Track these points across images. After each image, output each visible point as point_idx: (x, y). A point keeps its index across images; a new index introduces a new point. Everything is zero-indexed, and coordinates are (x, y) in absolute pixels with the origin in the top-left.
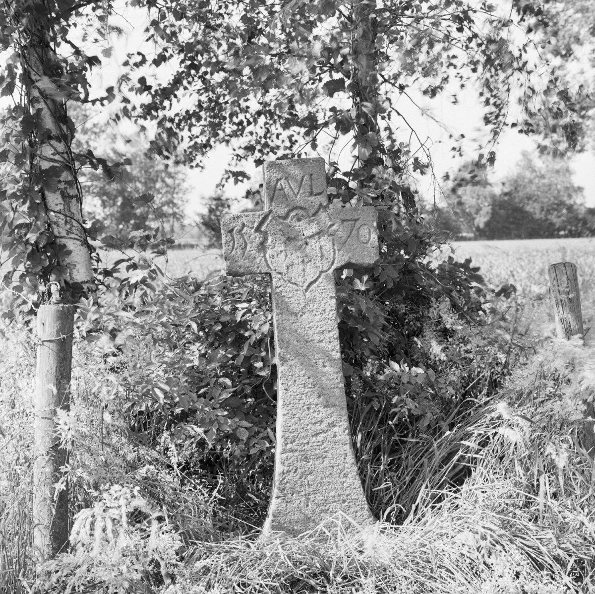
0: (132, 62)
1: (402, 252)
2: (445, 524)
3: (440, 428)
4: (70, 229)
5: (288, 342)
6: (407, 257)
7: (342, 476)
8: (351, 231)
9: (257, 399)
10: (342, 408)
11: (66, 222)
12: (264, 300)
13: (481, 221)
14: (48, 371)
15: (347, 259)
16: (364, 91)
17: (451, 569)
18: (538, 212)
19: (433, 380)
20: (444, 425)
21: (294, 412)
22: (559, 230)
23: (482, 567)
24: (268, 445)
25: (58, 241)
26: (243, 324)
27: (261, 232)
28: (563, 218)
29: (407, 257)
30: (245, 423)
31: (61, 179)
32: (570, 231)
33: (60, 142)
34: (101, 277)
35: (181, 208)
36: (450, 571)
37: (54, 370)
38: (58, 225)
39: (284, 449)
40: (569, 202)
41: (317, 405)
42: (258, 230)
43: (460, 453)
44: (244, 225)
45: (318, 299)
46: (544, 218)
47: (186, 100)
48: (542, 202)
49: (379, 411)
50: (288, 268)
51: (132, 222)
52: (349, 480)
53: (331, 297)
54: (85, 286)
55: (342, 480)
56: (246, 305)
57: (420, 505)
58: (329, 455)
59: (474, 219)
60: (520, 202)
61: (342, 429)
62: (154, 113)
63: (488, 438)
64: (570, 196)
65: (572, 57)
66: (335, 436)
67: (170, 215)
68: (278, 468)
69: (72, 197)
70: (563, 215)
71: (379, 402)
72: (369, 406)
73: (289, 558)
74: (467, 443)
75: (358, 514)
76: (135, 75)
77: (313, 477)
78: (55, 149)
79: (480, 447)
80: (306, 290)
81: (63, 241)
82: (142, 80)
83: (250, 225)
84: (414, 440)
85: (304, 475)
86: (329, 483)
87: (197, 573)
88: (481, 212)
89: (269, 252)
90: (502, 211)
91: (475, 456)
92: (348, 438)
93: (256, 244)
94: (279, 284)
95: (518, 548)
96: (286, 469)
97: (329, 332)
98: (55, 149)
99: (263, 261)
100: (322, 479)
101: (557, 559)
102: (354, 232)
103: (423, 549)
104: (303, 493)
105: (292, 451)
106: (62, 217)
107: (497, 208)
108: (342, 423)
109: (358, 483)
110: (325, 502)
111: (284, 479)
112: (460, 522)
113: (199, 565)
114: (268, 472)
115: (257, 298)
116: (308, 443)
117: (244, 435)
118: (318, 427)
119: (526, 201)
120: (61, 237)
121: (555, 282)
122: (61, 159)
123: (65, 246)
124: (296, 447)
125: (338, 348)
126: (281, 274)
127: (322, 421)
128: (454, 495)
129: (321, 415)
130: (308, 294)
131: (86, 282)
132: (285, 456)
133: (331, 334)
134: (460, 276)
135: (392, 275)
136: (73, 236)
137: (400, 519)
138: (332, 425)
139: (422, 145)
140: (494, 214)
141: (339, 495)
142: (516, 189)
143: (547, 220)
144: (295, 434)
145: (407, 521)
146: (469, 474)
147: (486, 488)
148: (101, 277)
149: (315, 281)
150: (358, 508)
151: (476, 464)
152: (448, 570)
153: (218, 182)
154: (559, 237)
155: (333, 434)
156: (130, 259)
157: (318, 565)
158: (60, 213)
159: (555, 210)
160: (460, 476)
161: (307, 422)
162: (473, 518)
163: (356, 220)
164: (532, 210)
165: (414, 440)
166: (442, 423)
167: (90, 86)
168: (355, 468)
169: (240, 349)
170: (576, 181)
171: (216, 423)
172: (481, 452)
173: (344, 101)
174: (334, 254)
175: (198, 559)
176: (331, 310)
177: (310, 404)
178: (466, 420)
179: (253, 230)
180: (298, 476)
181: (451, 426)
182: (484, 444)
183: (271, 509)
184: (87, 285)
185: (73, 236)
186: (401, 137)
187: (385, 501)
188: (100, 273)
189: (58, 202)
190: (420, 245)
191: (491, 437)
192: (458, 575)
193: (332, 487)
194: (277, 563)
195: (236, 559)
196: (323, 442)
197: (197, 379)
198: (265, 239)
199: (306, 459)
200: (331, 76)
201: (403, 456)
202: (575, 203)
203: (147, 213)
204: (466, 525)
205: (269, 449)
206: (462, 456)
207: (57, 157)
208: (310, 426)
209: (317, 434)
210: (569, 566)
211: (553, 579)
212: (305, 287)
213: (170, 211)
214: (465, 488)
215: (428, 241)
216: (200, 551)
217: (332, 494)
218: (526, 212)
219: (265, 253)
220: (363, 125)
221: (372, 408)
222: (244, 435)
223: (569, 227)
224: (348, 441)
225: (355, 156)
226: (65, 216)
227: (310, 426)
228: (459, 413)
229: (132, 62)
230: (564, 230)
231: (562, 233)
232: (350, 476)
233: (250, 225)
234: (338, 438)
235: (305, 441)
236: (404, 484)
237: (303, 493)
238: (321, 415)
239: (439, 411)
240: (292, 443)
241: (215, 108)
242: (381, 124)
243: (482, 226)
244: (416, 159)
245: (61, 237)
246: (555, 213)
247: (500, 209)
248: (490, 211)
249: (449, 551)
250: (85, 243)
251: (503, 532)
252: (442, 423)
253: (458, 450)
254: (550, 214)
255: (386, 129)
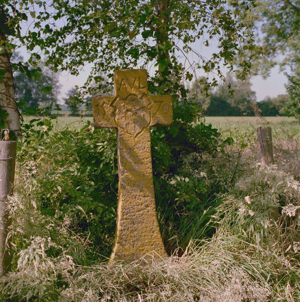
0: (42, 16)
1: (180, 120)
2: (205, 257)
3: (200, 208)
4: (9, 102)
5: (126, 163)
6: (182, 122)
7: (151, 232)
8: (159, 107)
9: (108, 193)
10: (153, 198)
11: (7, 99)
12: (113, 141)
13: (205, 107)
14: (2, 176)
15: (157, 121)
16: (162, 37)
17: (209, 280)
18: (233, 103)
19: (197, 184)
20: (202, 207)
21: (128, 199)
22: (243, 112)
23: (225, 279)
24: (113, 216)
25: (2, 108)
26: (101, 154)
27: (113, 106)
28: (245, 107)
29: (182, 122)
30: (101, 205)
31: (5, 76)
32: (248, 113)
33: (5, 57)
34: (23, 128)
35: (55, 96)
36: (209, 282)
37: (5, 176)
38: (3, 100)
39: (122, 218)
40: (248, 99)
41: (139, 196)
42: (111, 105)
43: (210, 221)
44: (104, 103)
45: (141, 142)
46: (236, 106)
47: (70, 38)
48: (235, 98)
49: (168, 200)
50: (126, 126)
51: (30, 102)
52: (155, 234)
53: (148, 141)
54: (16, 133)
55: (151, 234)
56: (102, 144)
57: (190, 247)
58: (145, 221)
59: (202, 106)
60: (225, 98)
61: (152, 208)
62: (53, 44)
63: (224, 214)
64: (249, 96)
65: (254, 27)
66: (148, 212)
67: (50, 99)
68: (119, 227)
69: (10, 86)
70: (245, 105)
71: (169, 195)
72: (164, 197)
73: (127, 274)
74: (213, 216)
75: (159, 252)
76: (43, 24)
77: (137, 232)
78: (2, 60)
79: (220, 219)
80: (136, 137)
81: (5, 108)
82: (47, 26)
83: (108, 103)
84: (186, 214)
85: (132, 231)
86: (145, 236)
87: (80, 282)
88: (205, 103)
89: (117, 117)
90: (216, 102)
91: (218, 222)
92: (155, 212)
93: (110, 113)
94: (121, 134)
95: (243, 269)
96: (123, 228)
97: (147, 158)
98: (2, 60)
99: (114, 121)
100: (141, 233)
101: (262, 274)
102: (161, 107)
103: (193, 270)
104: (131, 241)
105: (126, 219)
106: (5, 96)
107: (213, 100)
108: (152, 205)
109: (159, 236)
110: (143, 245)
111: (122, 233)
112: (212, 256)
113: (80, 278)
114: (112, 229)
115: (107, 141)
116: (134, 215)
117: (100, 211)
118: (140, 207)
119: (227, 97)
120: (4, 107)
121: (261, 136)
122: (5, 66)
123: (6, 111)
124: (128, 217)
125: (151, 167)
126: (123, 128)
127: (142, 204)
128: (209, 242)
129: (141, 201)
130: (136, 139)
131: (17, 131)
132: (122, 221)
133: (148, 160)
134: (209, 132)
135: (175, 132)
136: (10, 106)
137: (180, 254)
138: (147, 206)
139: (191, 65)
140: (212, 103)
141: (150, 242)
142: (223, 91)
143: (237, 107)
144: (128, 210)
145: (184, 255)
146: (215, 231)
147: (223, 239)
148: (23, 128)
149: (140, 132)
150: (159, 248)
151: (218, 226)
152: (208, 281)
153: (86, 82)
154: (244, 116)
155: (147, 210)
156: (39, 120)
157: (141, 278)
158: (4, 94)
159: (241, 102)
160: (210, 233)
161: (134, 204)
162: (219, 254)
163: (162, 102)
164: (230, 102)
165: (186, 214)
166: (201, 206)
167: (21, 28)
168: (158, 228)
169: (98, 166)
170: (253, 89)
171: (87, 204)
172: (221, 221)
173: (152, 42)
174: (150, 119)
175: (80, 275)
176: (148, 148)
177: (136, 195)
178: (215, 205)
179: (109, 105)
180: (129, 232)
181: (206, 208)
182: (222, 217)
183: (115, 249)
184: (17, 132)
185: (10, 106)
186: (180, 61)
187: (171, 245)
188: (24, 126)
189: (3, 88)
190: (191, 117)
191: (226, 213)
192: (212, 283)
193: (146, 237)
194: (121, 277)
195: (100, 274)
196: (142, 215)
197: (77, 182)
198: (115, 110)
199: (134, 223)
200: (144, 29)
201: (181, 222)
202: (251, 99)
203: (39, 98)
204: (216, 258)
205: (113, 218)
206: (211, 223)
207: (3, 65)
208: (135, 208)
209: (139, 211)
210: (268, 279)
211: (260, 285)
212: (135, 135)
213: (50, 97)
214: (214, 238)
215: (194, 114)
216: (81, 271)
217: (146, 241)
218: (227, 103)
219: (115, 117)
220: (161, 54)
221: (165, 197)
222: (100, 211)
223: (248, 111)
224: (155, 214)
225: (156, 71)
226: (7, 95)
227: (135, 208)
228: (210, 201)
229: (42, 16)
230: (246, 112)
231: (244, 114)
232: (155, 232)
233: (108, 103)
234: (150, 213)
235: (133, 214)
236: (181, 236)
237: (131, 241)
238: (141, 201)
239: (199, 200)
240: (126, 215)
241: (84, 44)
242: (171, 54)
243: (205, 109)
244: (188, 73)
245: (4, 107)
246: (241, 104)
247: (215, 101)
248: (210, 102)
249: (208, 271)
250: (17, 110)
251: (234, 261)
252: (201, 206)
253: (209, 219)
254: (239, 104)
255: (172, 57)
